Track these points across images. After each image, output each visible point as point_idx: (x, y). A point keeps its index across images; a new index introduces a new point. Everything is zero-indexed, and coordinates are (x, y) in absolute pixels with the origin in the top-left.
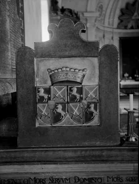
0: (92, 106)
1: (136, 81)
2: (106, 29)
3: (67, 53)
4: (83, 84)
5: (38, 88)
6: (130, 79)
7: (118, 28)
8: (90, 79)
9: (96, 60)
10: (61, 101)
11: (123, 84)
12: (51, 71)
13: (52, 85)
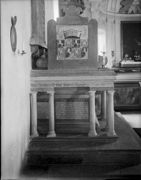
0: (85, 49)
1: (135, 61)
2: (109, 13)
3: (72, 23)
4: (80, 39)
5: (58, 40)
6: (129, 60)
7: (120, 12)
8: (84, 36)
9: (87, 27)
10: (70, 47)
11: (124, 64)
12: (65, 32)
13: (65, 39)
